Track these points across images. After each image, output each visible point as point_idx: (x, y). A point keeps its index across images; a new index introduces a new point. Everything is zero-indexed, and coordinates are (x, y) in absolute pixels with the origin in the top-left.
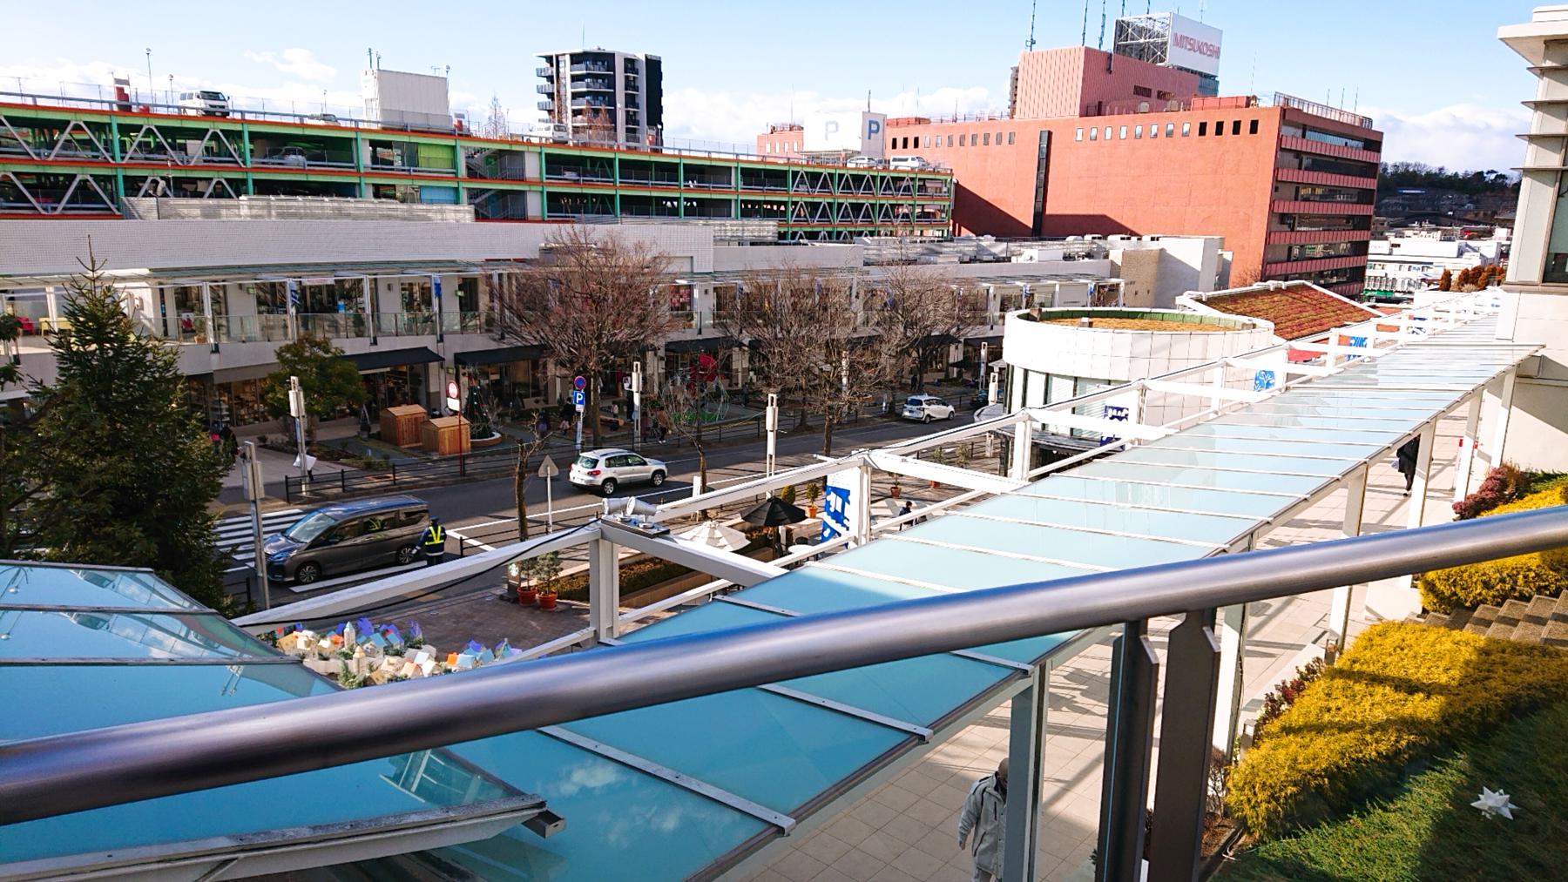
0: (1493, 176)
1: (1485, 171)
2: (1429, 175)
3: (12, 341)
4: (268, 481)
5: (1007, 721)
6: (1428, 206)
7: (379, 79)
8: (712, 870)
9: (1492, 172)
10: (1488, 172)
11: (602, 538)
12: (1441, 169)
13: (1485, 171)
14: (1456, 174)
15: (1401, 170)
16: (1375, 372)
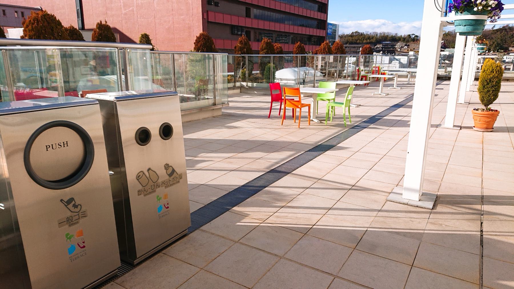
0: (414, 36)
1: (411, 34)
2: (392, 37)
3: (503, 6)
4: (454, 49)
5: (503, 81)
6: (391, 47)
7: (250, 16)
8: (512, 81)
9: (414, 34)
10: (412, 35)
11: (411, 63)
12: (396, 34)
13: (411, 34)
14: (401, 36)
15: (382, 35)
16: (299, 67)
